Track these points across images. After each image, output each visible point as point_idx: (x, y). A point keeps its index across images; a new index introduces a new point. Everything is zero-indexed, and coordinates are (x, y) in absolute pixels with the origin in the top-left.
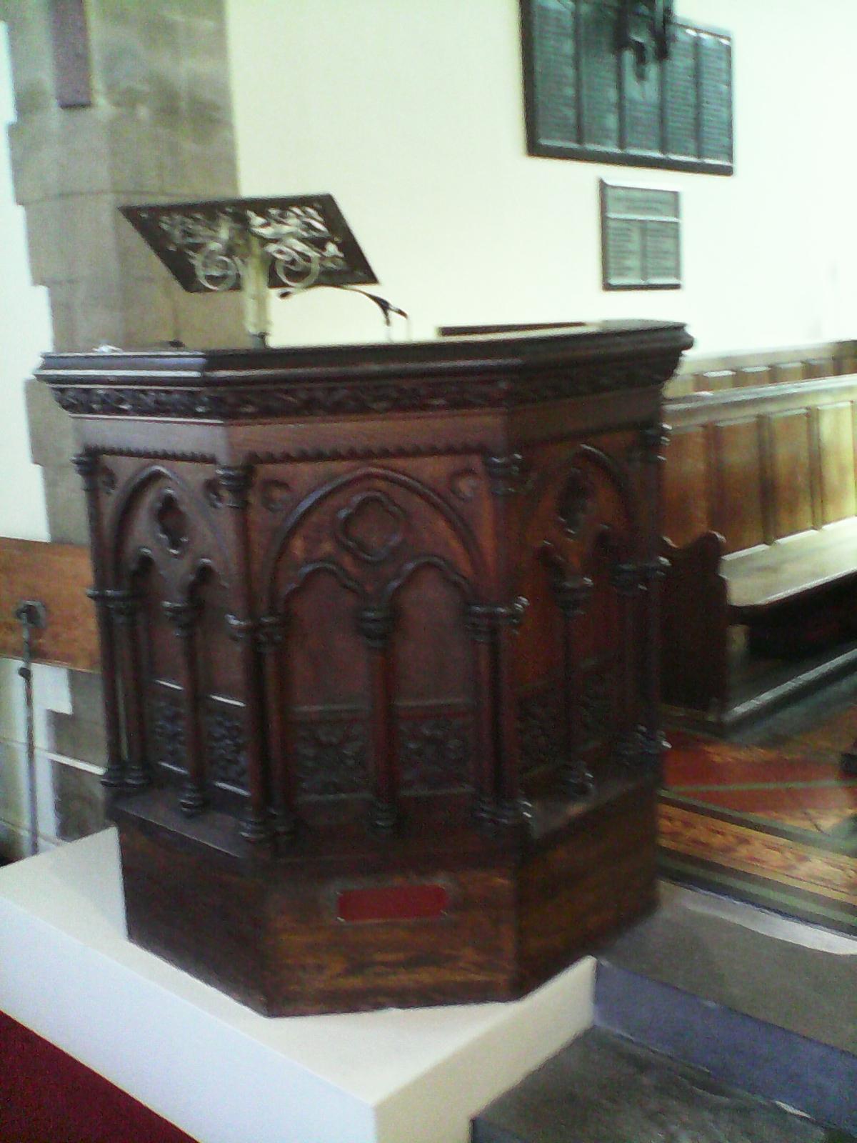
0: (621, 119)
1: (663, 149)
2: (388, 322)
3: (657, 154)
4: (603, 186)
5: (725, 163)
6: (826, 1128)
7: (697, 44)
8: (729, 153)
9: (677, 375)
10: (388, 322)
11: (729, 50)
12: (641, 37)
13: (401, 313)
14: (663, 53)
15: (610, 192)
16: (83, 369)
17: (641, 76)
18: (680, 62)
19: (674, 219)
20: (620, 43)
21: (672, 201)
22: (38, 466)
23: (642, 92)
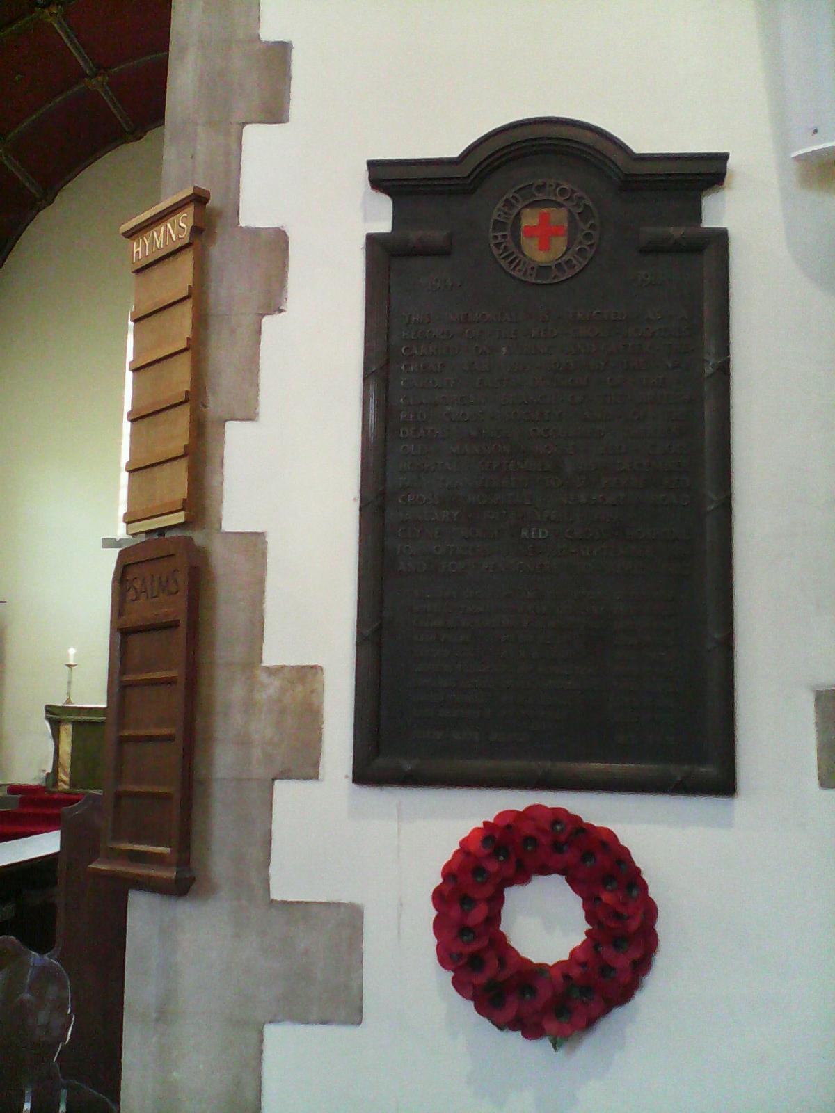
9: (254, 543)
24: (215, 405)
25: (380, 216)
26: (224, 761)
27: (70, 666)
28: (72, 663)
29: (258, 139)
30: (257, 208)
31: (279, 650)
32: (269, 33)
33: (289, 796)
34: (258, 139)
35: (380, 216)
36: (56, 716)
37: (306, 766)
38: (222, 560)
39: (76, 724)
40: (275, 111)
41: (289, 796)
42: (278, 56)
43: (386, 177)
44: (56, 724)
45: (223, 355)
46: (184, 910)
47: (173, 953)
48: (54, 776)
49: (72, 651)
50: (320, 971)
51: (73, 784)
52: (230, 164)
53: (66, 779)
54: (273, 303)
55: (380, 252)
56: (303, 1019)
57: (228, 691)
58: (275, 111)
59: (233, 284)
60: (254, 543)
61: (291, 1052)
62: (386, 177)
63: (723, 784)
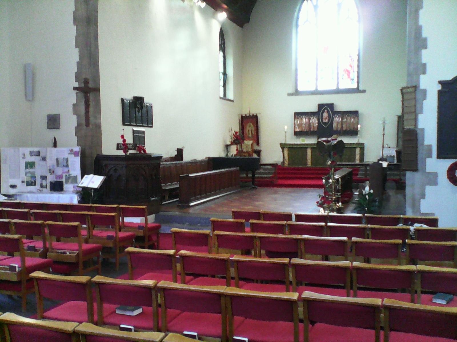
0: (136, 119)
1: (142, 124)
2: (122, 137)
3: (141, 125)
4: (133, 130)
5: (152, 126)
6: (31, 111)
7: (147, 106)
8: (152, 124)
9: (423, 130)
10: (122, 137)
11: (152, 107)
12: (138, 106)
13: (316, 7)
14: (142, 108)
15: (134, 131)
16: (180, 228)
17: (139, 112)
18: (144, 109)
19: (143, 135)
20: (136, 107)
21: (143, 132)
22: (176, 153)
23: (139, 114)
24: (417, 112)
25: (440, 87)
26: (420, 156)
27: (285, 132)
28: (286, 131)
29: (422, 77)
30: (422, 86)
31: (426, 143)
32: (424, 61)
33: (428, 160)
34: (422, 77)
35: (440, 87)
36: (283, 146)
37: (430, 156)
38: (418, 131)
39: (289, 148)
40: (424, 73)
41: (428, 160)
42: (425, 65)
43: (440, 82)
44: (283, 148)
45: (418, 106)
46: (415, 173)
47: (411, 178)
48: (283, 162)
49: (286, 127)
50: (433, 179)
51: (289, 164)
52: (418, 81)
53: (287, 163)
54: (425, 99)
55: (440, 92)
56: (430, 185)
57: (420, 148)
58: (424, 73)
59: (419, 96)
60: (423, 130)
61: (429, 189)
62: (440, 82)
63: (59, 115)
